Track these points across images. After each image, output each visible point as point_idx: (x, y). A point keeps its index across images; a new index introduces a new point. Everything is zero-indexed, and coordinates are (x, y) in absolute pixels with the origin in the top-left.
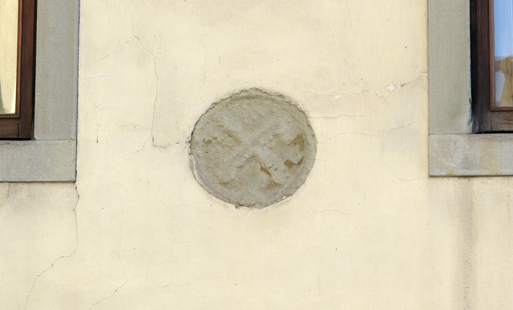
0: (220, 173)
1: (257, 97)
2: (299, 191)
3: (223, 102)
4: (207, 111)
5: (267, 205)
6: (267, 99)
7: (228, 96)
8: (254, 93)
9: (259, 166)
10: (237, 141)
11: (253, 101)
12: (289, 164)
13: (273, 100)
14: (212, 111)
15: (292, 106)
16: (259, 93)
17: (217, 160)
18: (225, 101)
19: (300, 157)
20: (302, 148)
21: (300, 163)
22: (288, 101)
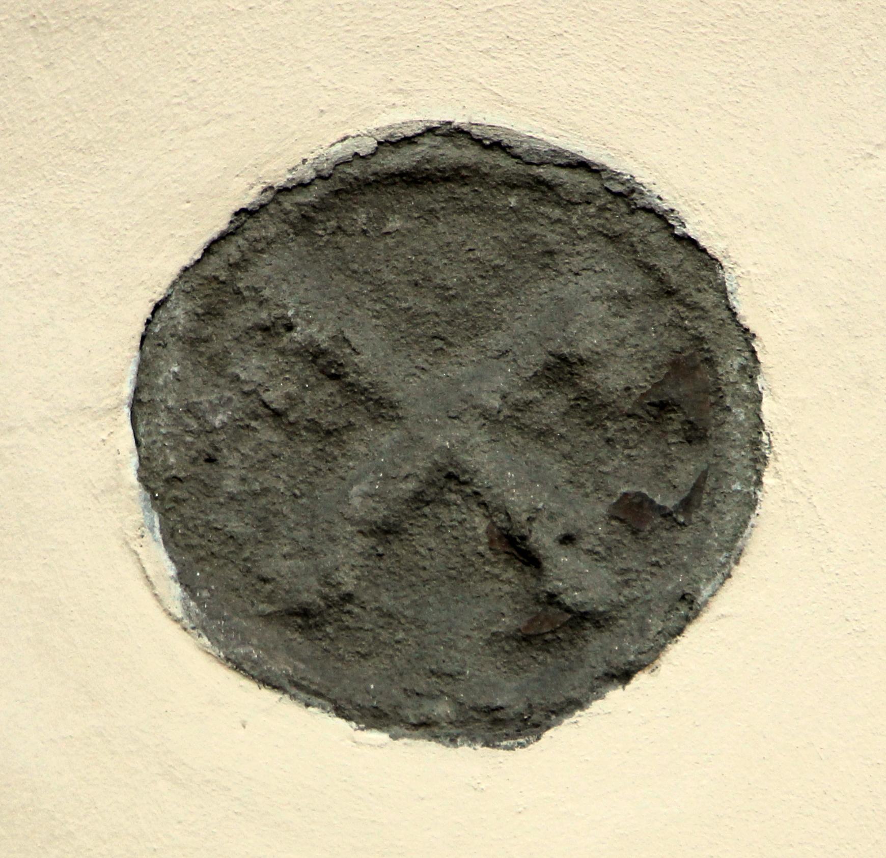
0: (280, 564)
1: (456, 175)
2: (161, 564)
3: (287, 203)
4: (208, 251)
5: (680, 631)
6: (511, 185)
7: (310, 174)
8: (451, 154)
9: (481, 524)
10: (381, 407)
11: (442, 191)
12: (633, 513)
13: (542, 188)
14: (232, 250)
15: (641, 218)
16: (471, 155)
17: (263, 501)
18: (300, 198)
19: (685, 473)
20: (695, 435)
21: (687, 504)
22: (618, 188)
